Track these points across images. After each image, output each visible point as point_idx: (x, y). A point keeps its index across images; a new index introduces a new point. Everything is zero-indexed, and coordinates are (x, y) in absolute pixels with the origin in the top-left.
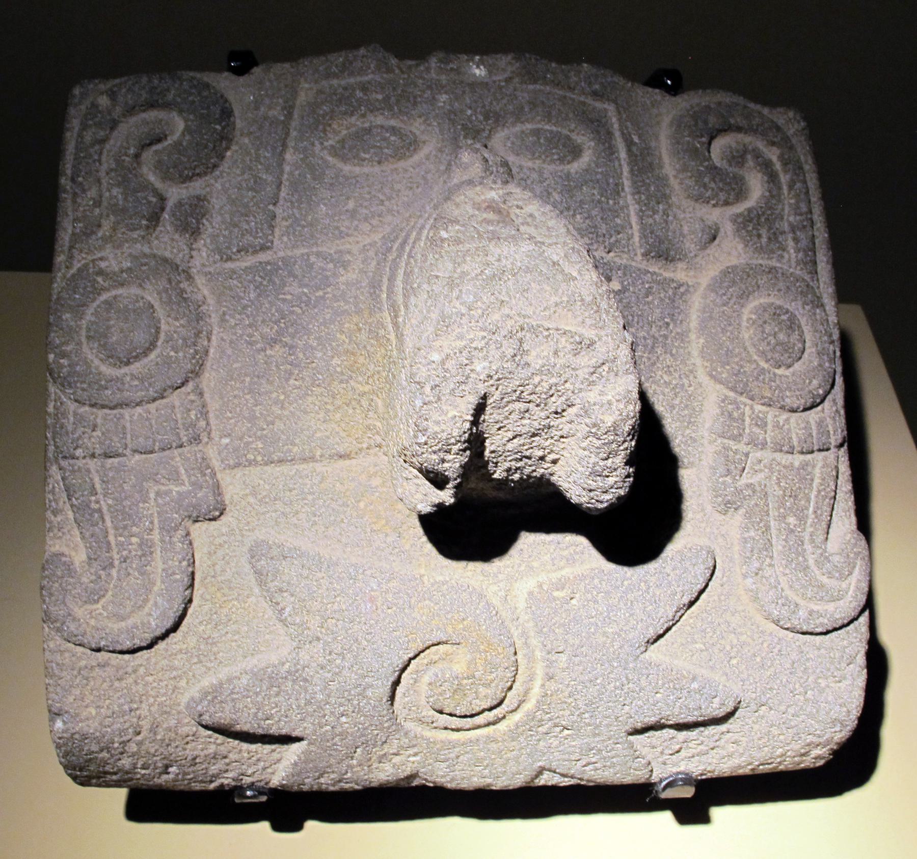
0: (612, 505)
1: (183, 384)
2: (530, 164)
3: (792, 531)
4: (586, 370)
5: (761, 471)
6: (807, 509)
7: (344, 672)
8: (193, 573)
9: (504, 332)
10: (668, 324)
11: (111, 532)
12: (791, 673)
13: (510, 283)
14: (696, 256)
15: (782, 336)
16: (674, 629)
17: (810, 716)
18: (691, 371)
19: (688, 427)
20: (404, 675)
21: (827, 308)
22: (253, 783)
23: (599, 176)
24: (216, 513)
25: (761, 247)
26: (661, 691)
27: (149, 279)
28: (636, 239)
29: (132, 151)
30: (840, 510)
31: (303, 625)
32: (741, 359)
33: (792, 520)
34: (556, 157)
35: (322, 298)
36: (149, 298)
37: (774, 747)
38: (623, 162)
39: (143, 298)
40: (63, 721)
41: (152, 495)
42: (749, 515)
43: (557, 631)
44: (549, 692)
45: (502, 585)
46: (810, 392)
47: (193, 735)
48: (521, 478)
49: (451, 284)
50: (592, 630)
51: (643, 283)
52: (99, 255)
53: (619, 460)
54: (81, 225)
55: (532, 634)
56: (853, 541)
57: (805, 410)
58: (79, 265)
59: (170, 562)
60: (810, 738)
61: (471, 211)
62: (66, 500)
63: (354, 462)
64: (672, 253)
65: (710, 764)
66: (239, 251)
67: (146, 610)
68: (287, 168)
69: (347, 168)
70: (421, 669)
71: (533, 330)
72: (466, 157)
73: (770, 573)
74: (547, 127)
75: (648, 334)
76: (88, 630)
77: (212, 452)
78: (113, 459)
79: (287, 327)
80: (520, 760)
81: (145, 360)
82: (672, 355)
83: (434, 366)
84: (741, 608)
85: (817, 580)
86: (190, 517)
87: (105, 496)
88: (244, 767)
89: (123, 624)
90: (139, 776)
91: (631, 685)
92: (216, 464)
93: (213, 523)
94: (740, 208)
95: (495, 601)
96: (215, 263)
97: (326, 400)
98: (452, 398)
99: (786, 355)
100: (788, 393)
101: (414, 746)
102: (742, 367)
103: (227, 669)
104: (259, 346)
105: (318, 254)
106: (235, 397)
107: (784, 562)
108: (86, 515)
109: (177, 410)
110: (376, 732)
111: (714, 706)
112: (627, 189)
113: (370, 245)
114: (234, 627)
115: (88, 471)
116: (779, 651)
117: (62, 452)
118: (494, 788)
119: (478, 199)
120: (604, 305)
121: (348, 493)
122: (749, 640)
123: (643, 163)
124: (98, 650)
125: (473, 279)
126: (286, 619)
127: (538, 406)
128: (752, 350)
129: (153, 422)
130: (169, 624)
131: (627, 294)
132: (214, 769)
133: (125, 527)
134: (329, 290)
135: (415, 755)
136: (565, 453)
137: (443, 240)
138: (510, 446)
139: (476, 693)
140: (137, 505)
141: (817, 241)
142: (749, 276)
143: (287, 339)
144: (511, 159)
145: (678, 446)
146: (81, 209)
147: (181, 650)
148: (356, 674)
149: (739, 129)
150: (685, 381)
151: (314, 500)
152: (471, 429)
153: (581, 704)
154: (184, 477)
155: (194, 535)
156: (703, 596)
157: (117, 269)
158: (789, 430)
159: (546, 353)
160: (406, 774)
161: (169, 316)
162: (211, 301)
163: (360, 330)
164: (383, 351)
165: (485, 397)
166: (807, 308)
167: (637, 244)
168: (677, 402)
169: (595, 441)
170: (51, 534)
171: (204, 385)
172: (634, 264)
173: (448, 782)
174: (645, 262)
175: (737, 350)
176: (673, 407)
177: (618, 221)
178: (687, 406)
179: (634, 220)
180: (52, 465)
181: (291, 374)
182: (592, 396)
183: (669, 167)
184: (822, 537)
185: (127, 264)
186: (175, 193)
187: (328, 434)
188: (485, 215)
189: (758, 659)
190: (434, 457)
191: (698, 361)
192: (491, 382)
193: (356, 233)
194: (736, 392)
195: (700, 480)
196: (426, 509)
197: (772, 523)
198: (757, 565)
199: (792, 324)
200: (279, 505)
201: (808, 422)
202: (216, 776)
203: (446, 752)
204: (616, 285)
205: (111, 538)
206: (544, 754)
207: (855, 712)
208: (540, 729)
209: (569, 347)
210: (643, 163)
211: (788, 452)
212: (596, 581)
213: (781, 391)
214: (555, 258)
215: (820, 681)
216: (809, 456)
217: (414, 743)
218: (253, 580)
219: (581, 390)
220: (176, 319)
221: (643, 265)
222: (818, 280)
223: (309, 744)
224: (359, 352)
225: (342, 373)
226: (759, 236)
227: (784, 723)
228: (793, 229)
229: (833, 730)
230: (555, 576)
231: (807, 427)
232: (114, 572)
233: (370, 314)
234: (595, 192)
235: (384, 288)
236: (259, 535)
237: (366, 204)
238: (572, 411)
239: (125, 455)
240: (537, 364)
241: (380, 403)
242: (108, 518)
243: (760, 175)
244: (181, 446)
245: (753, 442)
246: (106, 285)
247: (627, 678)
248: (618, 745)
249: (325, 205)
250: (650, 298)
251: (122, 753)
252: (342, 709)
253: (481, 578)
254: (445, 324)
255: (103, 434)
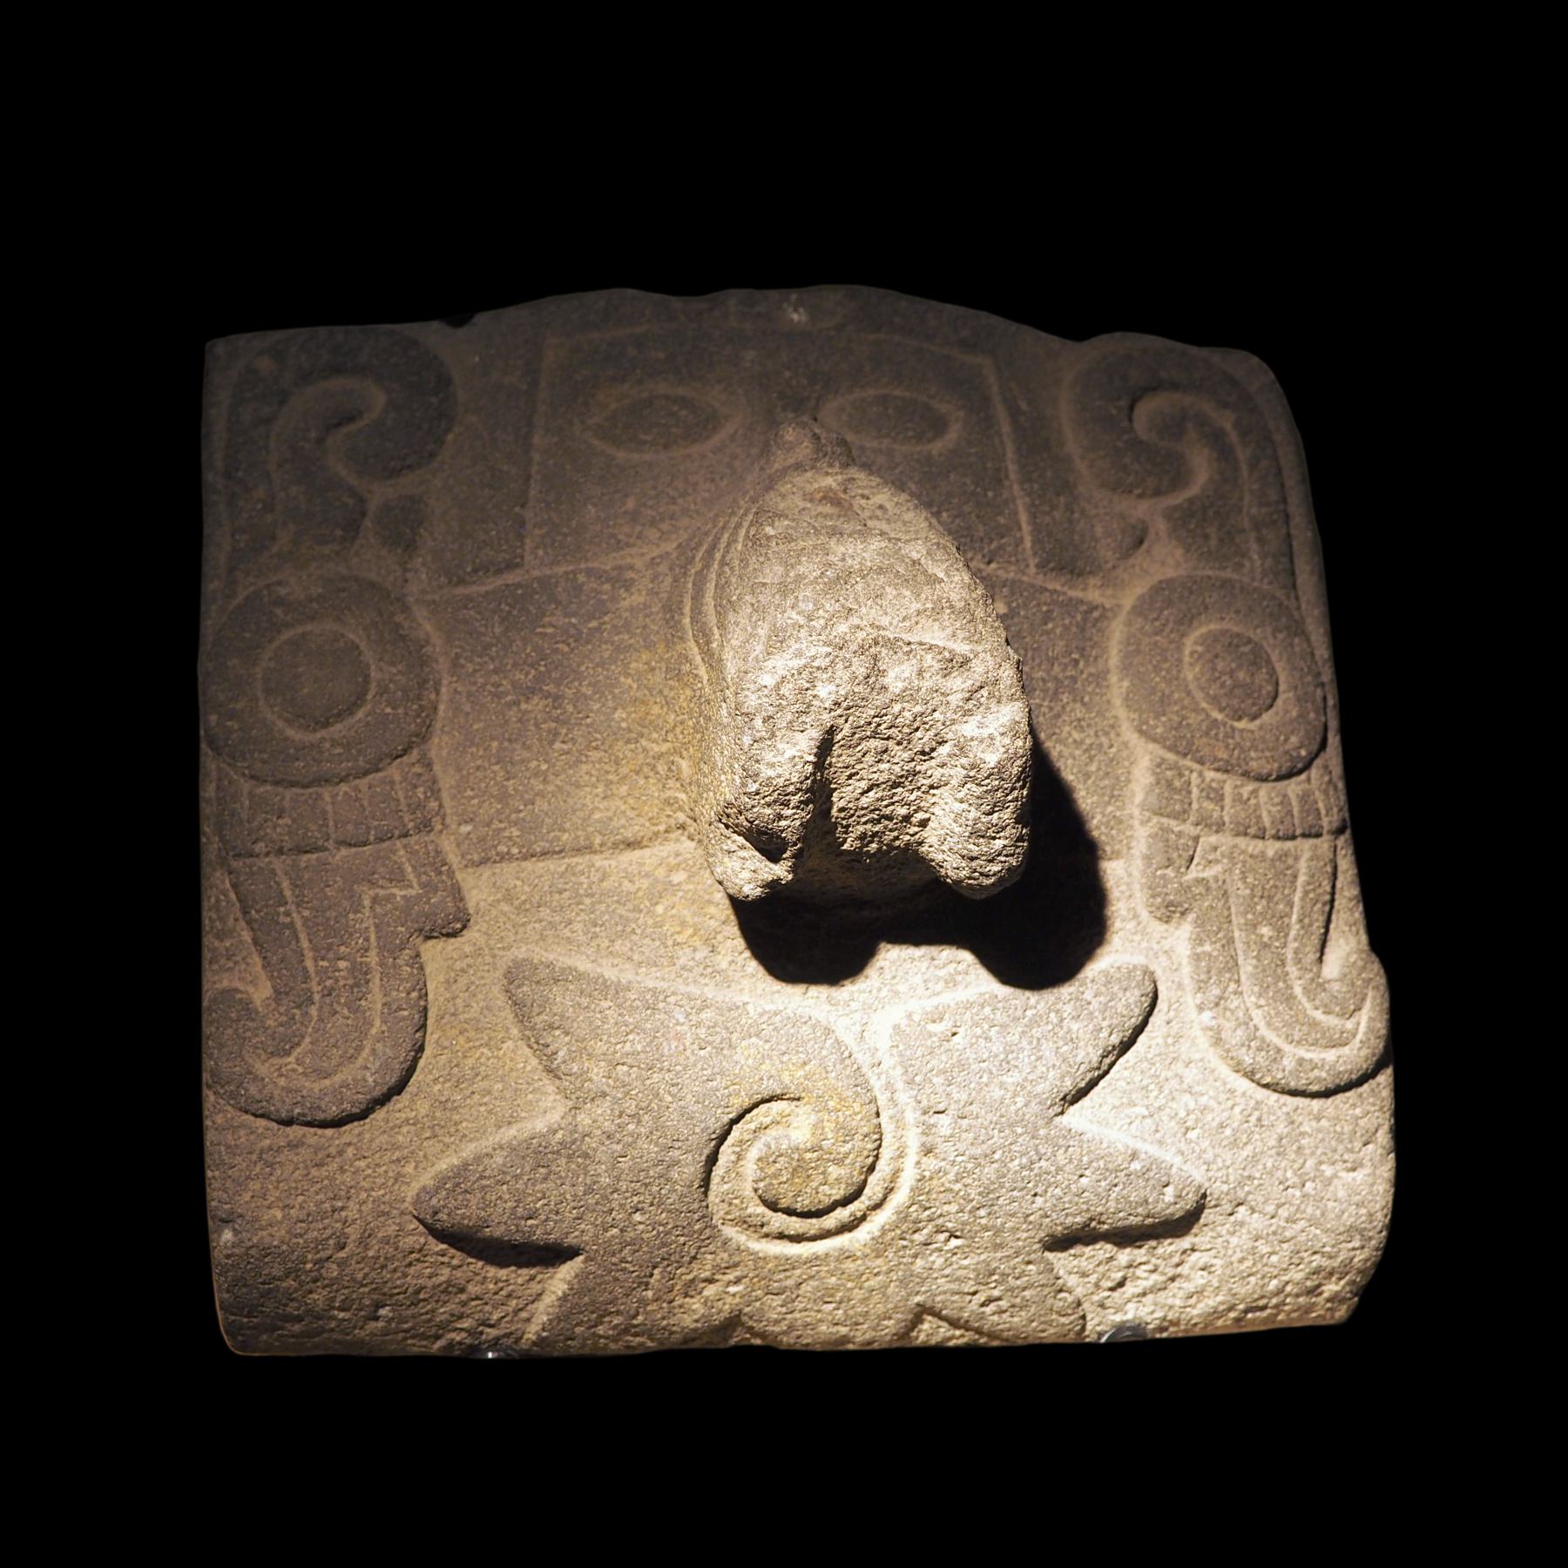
0: (1001, 880)
1: (405, 752)
2: (875, 444)
3: (1266, 946)
4: (960, 696)
5: (1217, 861)
6: (1289, 915)
7: (640, 1142)
8: (425, 1009)
9: (854, 647)
10: (1076, 662)
11: (309, 955)
12: (1278, 1154)
13: (859, 587)
14: (1114, 567)
15: (1241, 675)
16: (1102, 1083)
17: (1313, 1222)
18: (1113, 727)
19: (1109, 803)
20: (722, 1148)
21: (1313, 638)
22: (498, 1339)
23: (972, 459)
24: (453, 925)
25: (1210, 552)
26: (1087, 1173)
27: (349, 609)
28: (1028, 543)
29: (313, 435)
30: (1341, 922)
31: (583, 1075)
32: (1183, 708)
33: (1265, 931)
34: (910, 433)
35: (598, 629)
36: (352, 636)
37: (1263, 1277)
38: (1006, 439)
39: (343, 636)
40: (234, 1230)
41: (367, 903)
42: (1200, 923)
43: (935, 1080)
44: (927, 1174)
45: (856, 1016)
46: (1287, 752)
47: (420, 1250)
48: (879, 849)
49: (784, 590)
50: (985, 1079)
51: (1038, 605)
52: (275, 579)
53: (1007, 815)
54: (245, 537)
55: (900, 1085)
56: (1360, 963)
57: (1280, 778)
58: (246, 593)
59: (394, 993)
60: (1317, 1260)
61: (801, 504)
62: (239, 915)
63: (647, 852)
64: (1080, 563)
65: (1171, 1307)
66: (475, 571)
67: (360, 1061)
68: (537, 457)
69: (621, 455)
70: (746, 1137)
71: (892, 644)
72: (790, 434)
73: (1236, 1003)
74: (897, 393)
75: (1048, 672)
76: (276, 1092)
77: (448, 846)
78: (309, 856)
79: (549, 672)
80: (890, 1291)
81: (351, 721)
82: (1084, 704)
83: (766, 692)
84: (1197, 1056)
85: (1306, 1016)
86: (421, 930)
87: (298, 906)
88: (488, 1308)
89: (327, 1082)
90: (333, 1324)
91: (1043, 1163)
92: (453, 859)
93: (452, 940)
94: (1179, 498)
95: (849, 1039)
96: (440, 587)
97: (607, 767)
98: (790, 733)
99: (1250, 701)
100: (1253, 754)
101: (736, 1265)
102: (1184, 718)
103: (472, 1146)
104: (509, 698)
105: (589, 572)
106: (478, 768)
107: (1256, 989)
108: (270, 937)
109: (397, 787)
110: (682, 1239)
111: (1167, 1199)
112: (1012, 476)
113: (661, 557)
114: (485, 1084)
115: (273, 872)
116: (1259, 1120)
117: (234, 848)
118: (851, 1347)
119: (809, 488)
120: (980, 613)
121: (640, 894)
122: (1212, 1103)
123: (1037, 443)
124: (288, 1122)
125: (811, 583)
126: (558, 1067)
127: (899, 743)
128: (1199, 695)
129: (365, 803)
130: (392, 1079)
131: (1016, 620)
132: (443, 1312)
133: (329, 948)
134: (606, 619)
135: (737, 1281)
136: (936, 810)
137: (769, 538)
138: (864, 801)
139: (823, 1173)
140: (346, 916)
141: (1295, 543)
142: (1191, 592)
143: (550, 688)
144: (850, 437)
145: (1097, 826)
146: (245, 515)
147: (407, 1120)
148: (656, 1144)
149: (1175, 386)
150: (1104, 739)
151: (593, 904)
152: (814, 774)
153: (973, 1193)
154: (411, 877)
155: (425, 957)
156: (1142, 1038)
157: (302, 597)
158: (1257, 806)
159: (907, 674)
160: (723, 1315)
161: (381, 659)
162: (437, 639)
163: (653, 669)
164: (688, 692)
165: (831, 731)
166: (1280, 636)
167: (1029, 552)
168: (1093, 768)
169: (974, 788)
170: (216, 967)
171: (433, 754)
172: (1025, 578)
173: (784, 1333)
174: (1041, 577)
175: (1176, 696)
176: (1087, 776)
177: (1002, 520)
178: (1107, 774)
179: (1023, 518)
180: (215, 870)
181: (557, 734)
182: (969, 728)
183: (1073, 443)
184: (1313, 956)
185: (317, 590)
186: (380, 494)
187: (610, 814)
188: (820, 509)
189: (1228, 1132)
190: (768, 811)
191: (1122, 713)
192: (839, 712)
193: (639, 542)
194: (1178, 753)
195: (1130, 875)
196: (751, 891)
197: (1237, 934)
198: (1216, 991)
199: (1258, 659)
200: (545, 912)
201: (1285, 796)
202: (445, 1327)
203: (782, 1276)
204: (1001, 608)
205: (309, 963)
206: (922, 1283)
207: (1379, 1216)
208: (916, 1236)
209: (937, 666)
210: (1037, 443)
211: (1255, 837)
212: (987, 1010)
213: (1242, 751)
214: (915, 556)
215: (1323, 1167)
216: (1289, 844)
217: (737, 1259)
218: (511, 1016)
219: (954, 722)
220: (393, 664)
221: (1039, 580)
222: (1297, 598)
223: (586, 1261)
224: (652, 700)
225: (629, 730)
226: (1206, 537)
227: (1274, 1233)
228: (1257, 527)
229: (1350, 1246)
230: (930, 1004)
231: (1285, 801)
232: (313, 1011)
233: (667, 646)
234: (968, 481)
235: (687, 610)
236: (521, 953)
237: (650, 503)
238: (943, 750)
239: (326, 849)
240: (896, 686)
241: (684, 764)
242: (303, 936)
243: (1206, 451)
244: (405, 835)
245: (1204, 822)
246: (289, 618)
247: (1037, 1153)
248: (1031, 1267)
249: (595, 505)
250: (1050, 626)
251: (315, 1281)
252: (636, 1199)
253: (828, 1007)
254: (778, 639)
255: (294, 821)
